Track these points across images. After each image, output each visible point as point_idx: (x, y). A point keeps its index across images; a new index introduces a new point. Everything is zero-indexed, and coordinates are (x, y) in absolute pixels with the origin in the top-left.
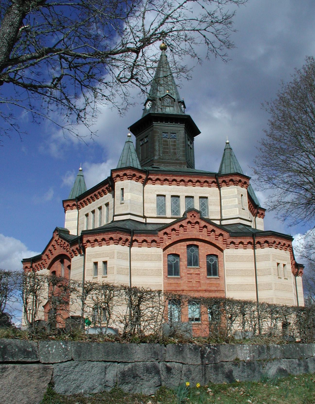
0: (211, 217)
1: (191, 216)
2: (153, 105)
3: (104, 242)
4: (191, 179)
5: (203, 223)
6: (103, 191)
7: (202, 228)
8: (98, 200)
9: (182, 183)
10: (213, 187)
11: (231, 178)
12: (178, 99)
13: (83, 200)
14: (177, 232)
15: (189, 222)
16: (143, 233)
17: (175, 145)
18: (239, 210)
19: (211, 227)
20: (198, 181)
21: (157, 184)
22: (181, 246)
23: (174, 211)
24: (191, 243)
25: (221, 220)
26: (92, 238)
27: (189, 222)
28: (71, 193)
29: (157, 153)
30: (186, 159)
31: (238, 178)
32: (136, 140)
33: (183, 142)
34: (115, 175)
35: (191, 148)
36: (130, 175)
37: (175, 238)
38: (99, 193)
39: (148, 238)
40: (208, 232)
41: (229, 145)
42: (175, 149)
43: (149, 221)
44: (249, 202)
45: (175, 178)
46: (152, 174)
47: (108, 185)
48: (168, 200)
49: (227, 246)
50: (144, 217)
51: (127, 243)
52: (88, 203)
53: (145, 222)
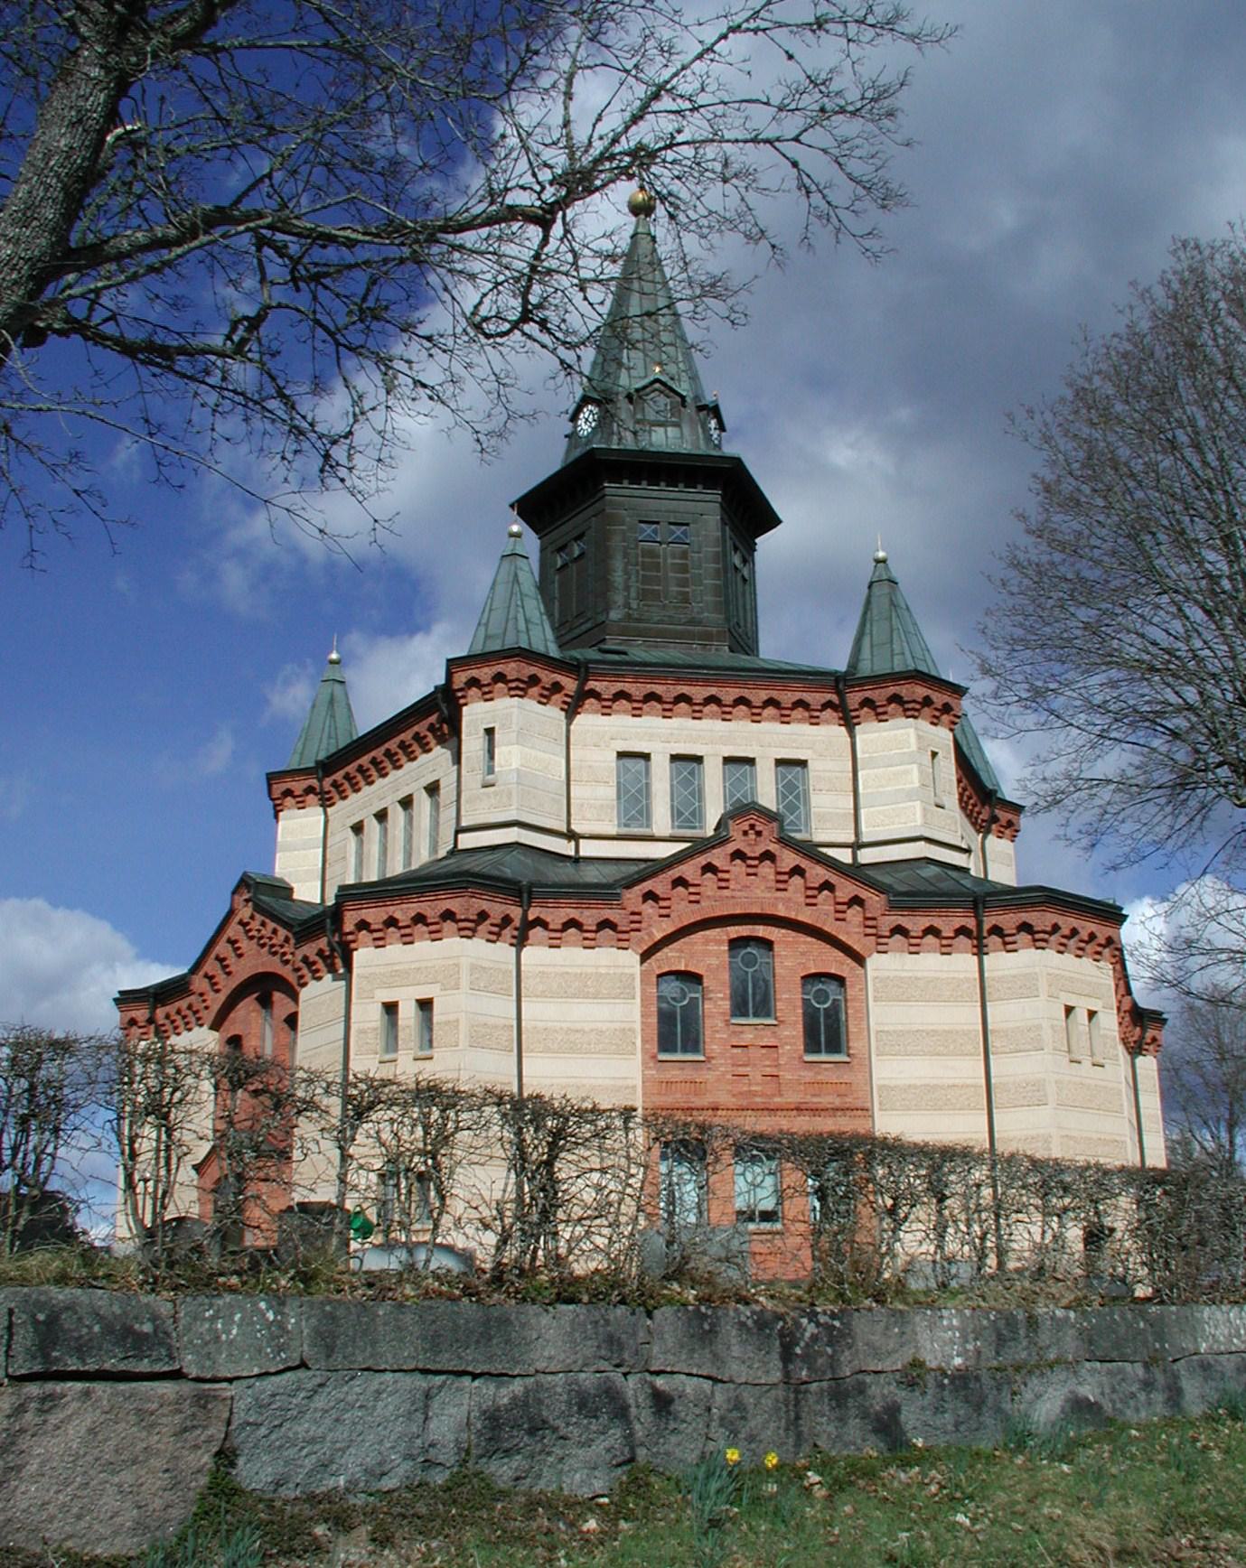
0: (819, 837)
1: (745, 833)
2: (605, 420)
3: (421, 928)
4: (746, 693)
5: (789, 859)
6: (418, 738)
8: (400, 772)
9: (713, 707)
10: (827, 722)
11: (892, 690)
12: (697, 398)
13: (342, 773)
14: (692, 890)
15: (738, 855)
16: (567, 895)
20: (771, 702)
21: (618, 712)
22: (707, 942)
23: (680, 814)
24: (744, 930)
25: (857, 846)
26: (375, 915)
27: (738, 855)
28: (300, 745)
29: (619, 598)
30: (727, 620)
31: (921, 691)
32: (543, 550)
34: (460, 678)
35: (745, 580)
37: (685, 913)
38: (403, 746)
39: (587, 912)
40: (810, 893)
41: (887, 569)
42: (684, 583)
43: (588, 849)
44: (959, 781)
45: (685, 689)
46: (601, 676)
47: (438, 716)
48: (661, 771)
49: (881, 943)
50: (571, 836)
51: (508, 932)
52: (362, 783)
53: (572, 853)
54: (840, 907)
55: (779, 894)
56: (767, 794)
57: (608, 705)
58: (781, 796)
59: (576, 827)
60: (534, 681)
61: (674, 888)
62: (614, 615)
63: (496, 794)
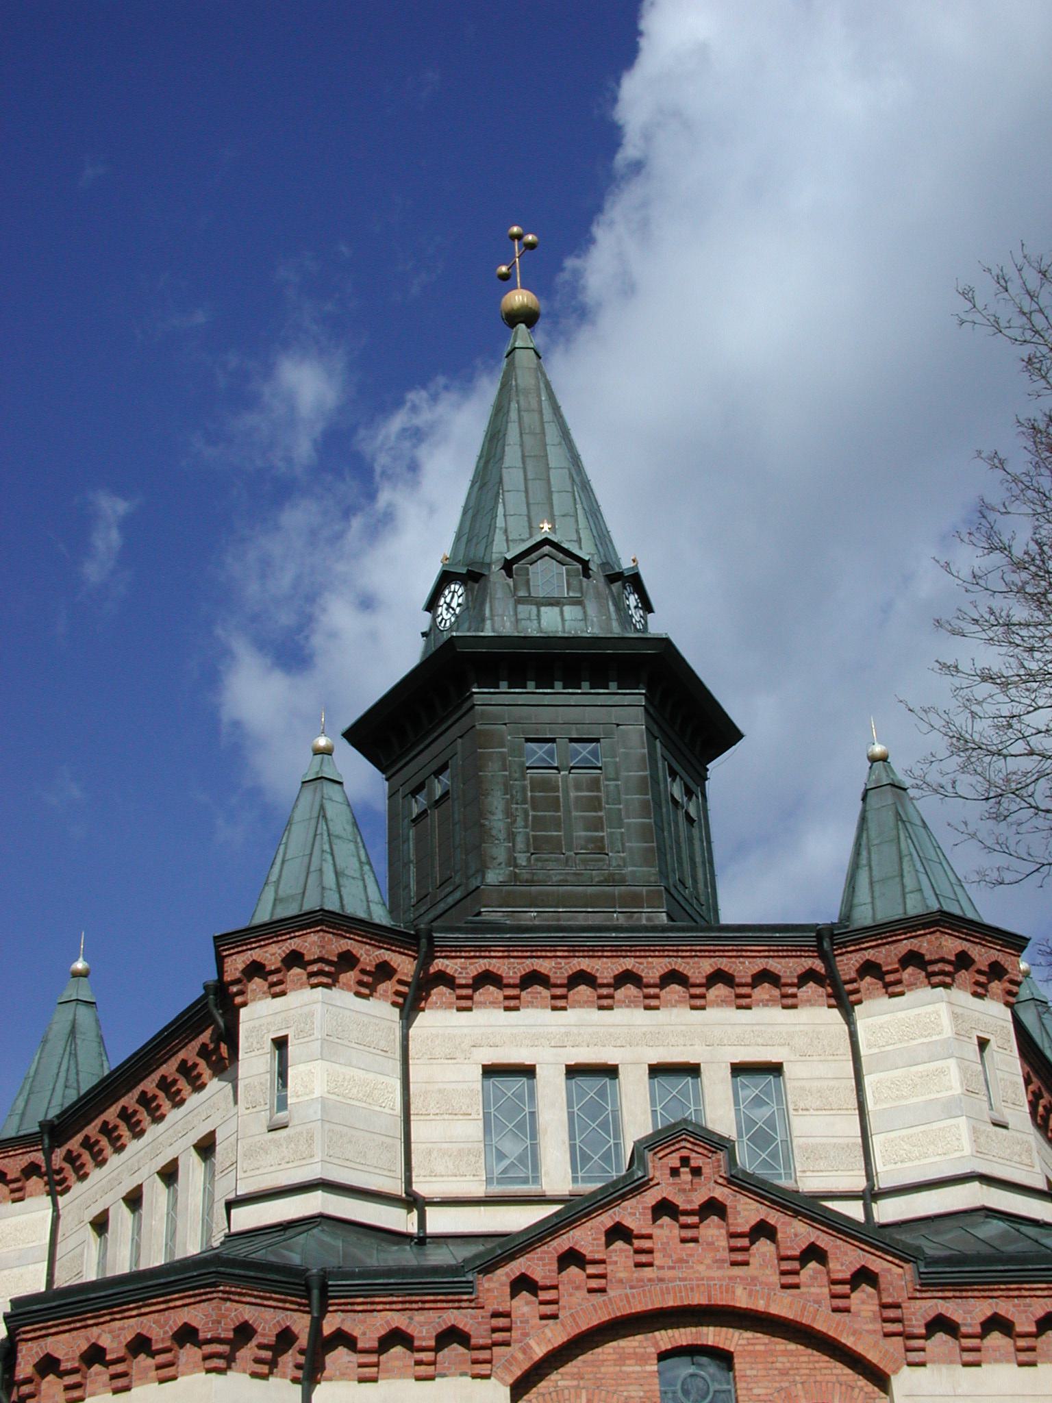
0: (809, 1183)
1: (675, 1172)
2: (474, 608)
3: (143, 1361)
4: (680, 965)
5: (747, 1212)
6: (186, 1070)
7: (745, 1242)
8: (162, 1126)
9: (630, 990)
10: (810, 1002)
11: (905, 946)
12: (604, 565)
13: (79, 1137)
14: (591, 1270)
15: (664, 1208)
16: (387, 1289)
17: (595, 804)
18: (975, 1130)
19: (796, 1233)
20: (719, 977)
21: (483, 1005)
22: (622, 1359)
23: (586, 1158)
25: (871, 1195)
26: (67, 1346)
27: (664, 1208)
28: (21, 1103)
29: (499, 852)
30: (663, 874)
31: (951, 945)
32: (392, 795)
33: (642, 786)
34: (236, 964)
35: (690, 820)
36: (321, 960)
37: (581, 1309)
38: (165, 1085)
39: (419, 1317)
40: (787, 1266)
41: (889, 770)
42: (597, 825)
43: (440, 1221)
44: (1028, 1082)
45: (585, 964)
46: (454, 951)
47: (204, 1035)
48: (551, 1089)
50: (413, 1202)
51: (289, 1359)
52: (109, 1150)
53: (413, 1229)
54: (839, 1289)
55: (737, 1271)
56: (719, 1110)
57: (466, 994)
58: (744, 1123)
59: (420, 1188)
60: (348, 960)
61: (561, 1269)
62: (493, 877)
63: (289, 1139)
